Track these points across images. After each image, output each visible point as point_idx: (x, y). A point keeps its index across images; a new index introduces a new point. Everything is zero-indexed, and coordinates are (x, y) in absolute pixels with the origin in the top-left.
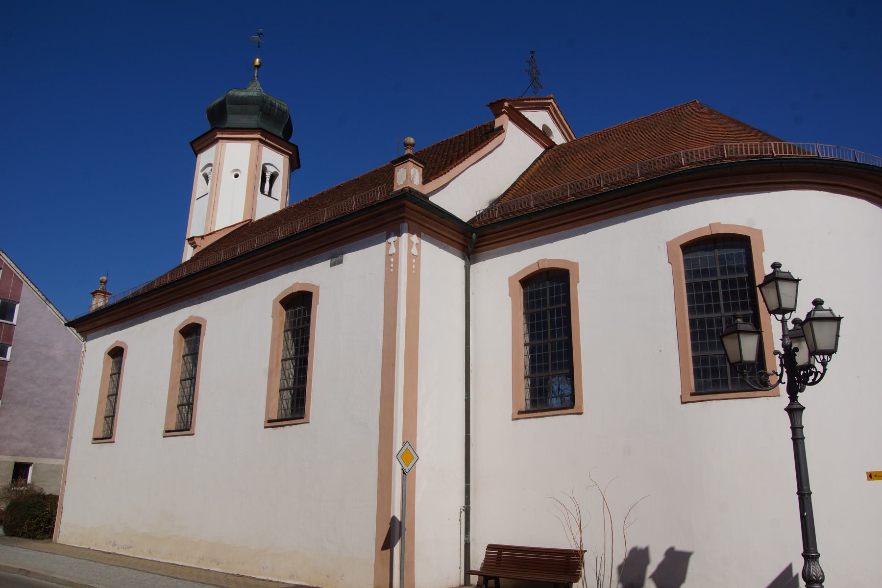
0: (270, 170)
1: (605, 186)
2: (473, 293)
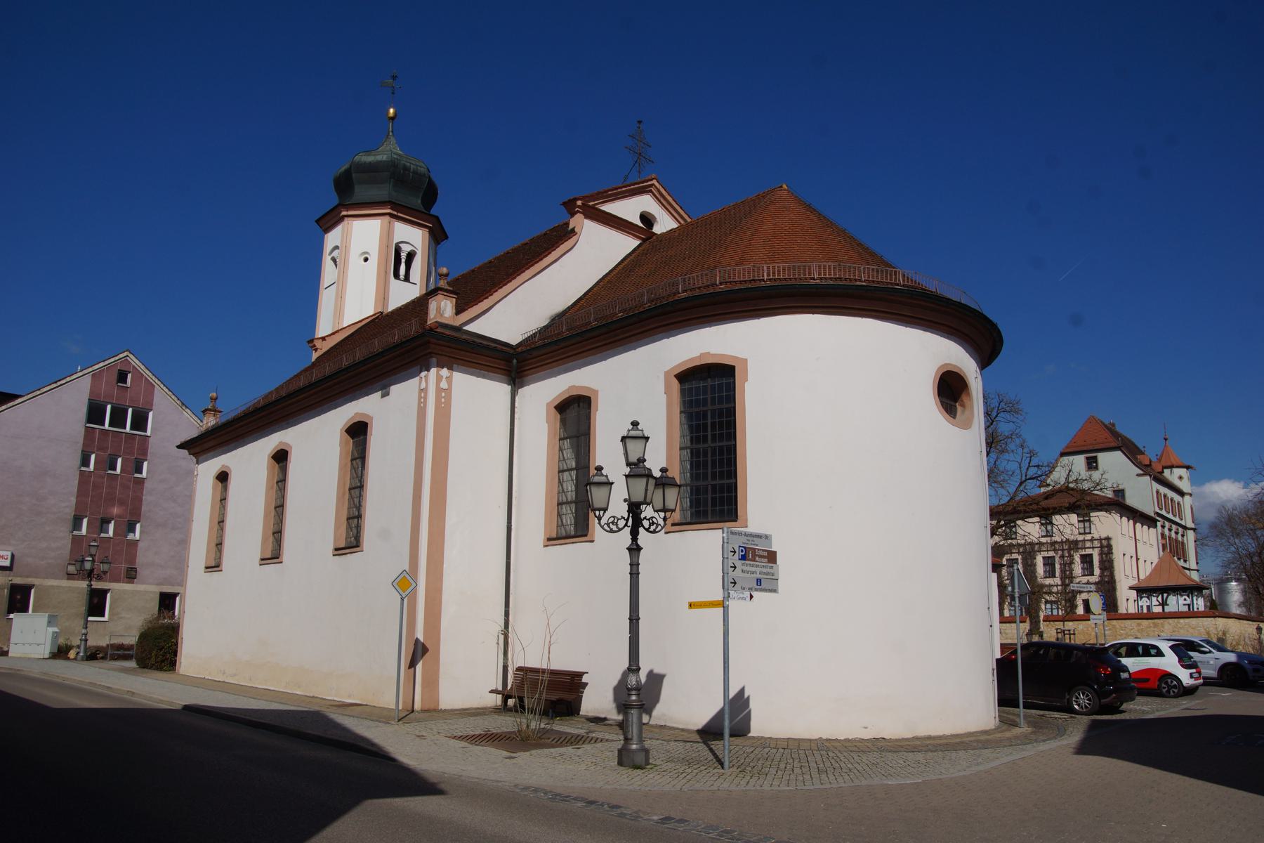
0: (406, 249)
1: (684, 291)
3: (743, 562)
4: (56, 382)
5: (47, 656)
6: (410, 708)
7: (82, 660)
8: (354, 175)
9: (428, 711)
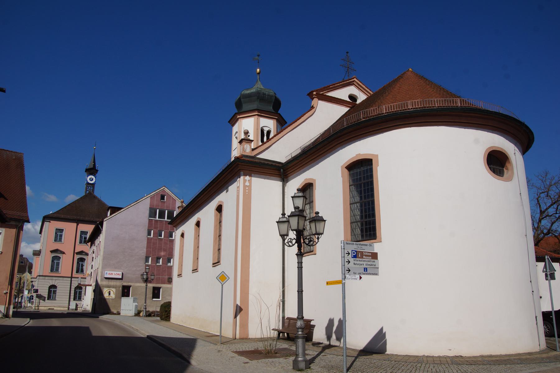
0: (266, 129)
2: (287, 197)
3: (355, 259)
4: (136, 202)
5: (133, 315)
6: (235, 338)
7: (145, 317)
8: (242, 100)
9: (243, 339)
